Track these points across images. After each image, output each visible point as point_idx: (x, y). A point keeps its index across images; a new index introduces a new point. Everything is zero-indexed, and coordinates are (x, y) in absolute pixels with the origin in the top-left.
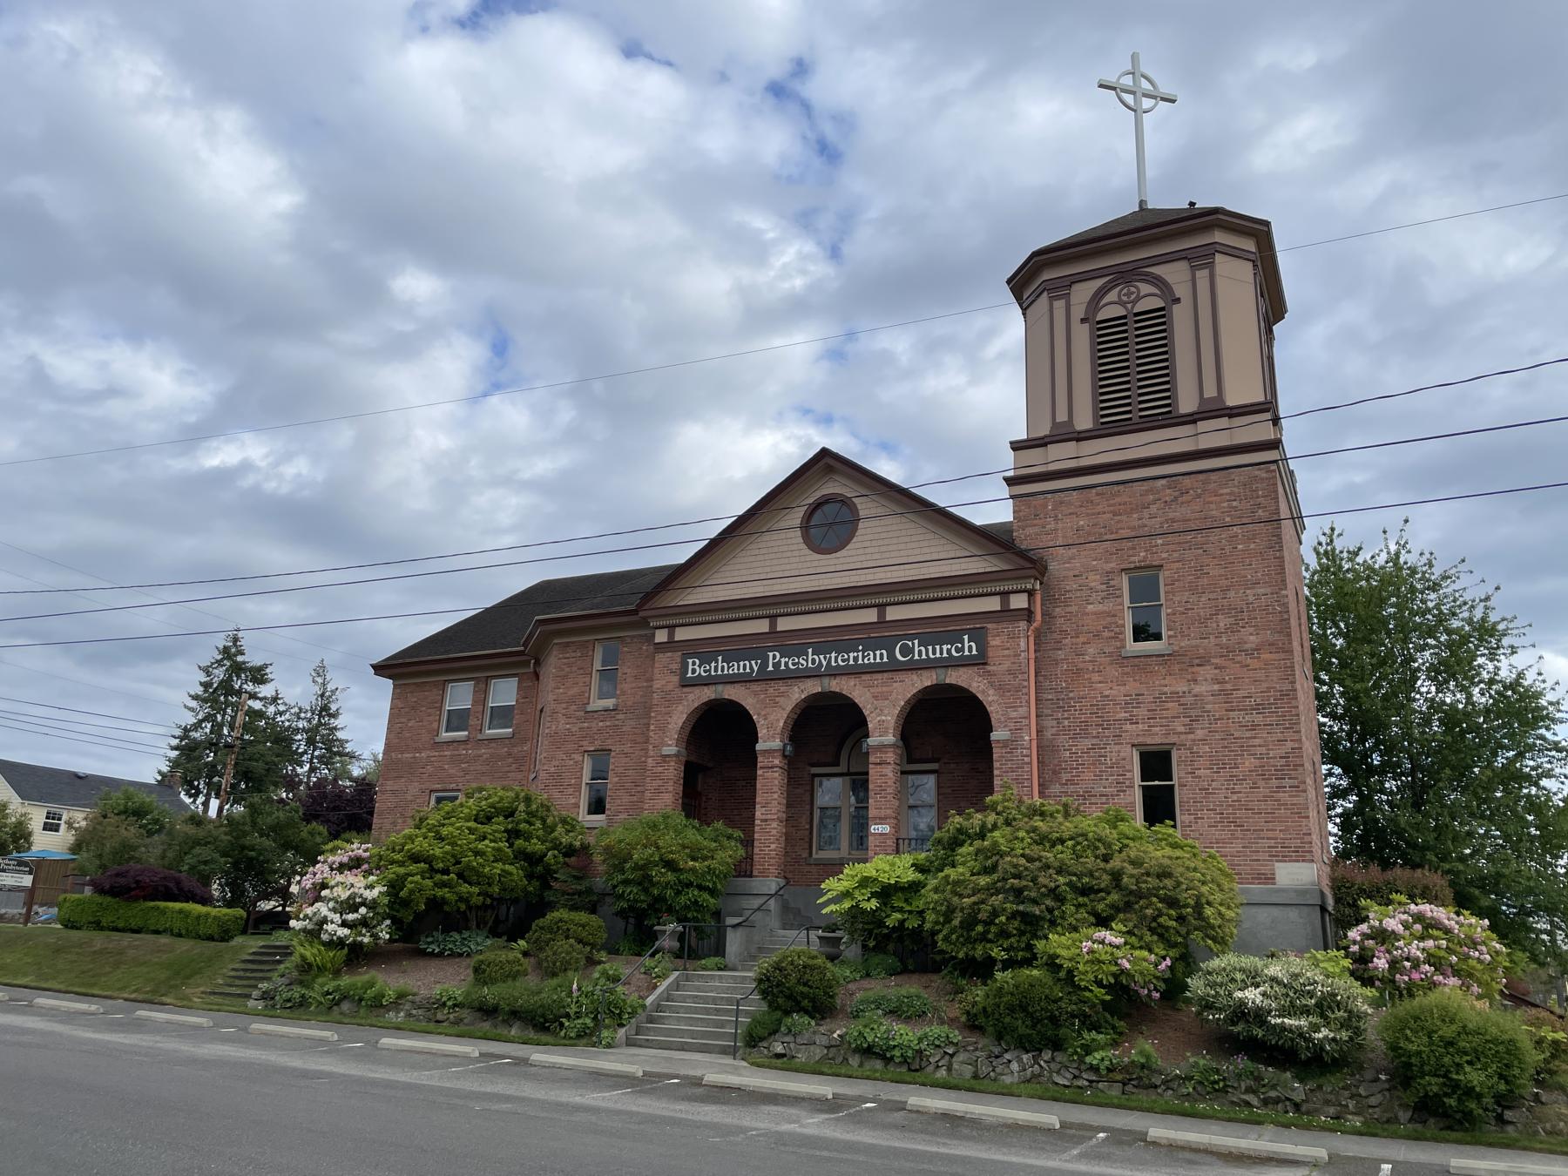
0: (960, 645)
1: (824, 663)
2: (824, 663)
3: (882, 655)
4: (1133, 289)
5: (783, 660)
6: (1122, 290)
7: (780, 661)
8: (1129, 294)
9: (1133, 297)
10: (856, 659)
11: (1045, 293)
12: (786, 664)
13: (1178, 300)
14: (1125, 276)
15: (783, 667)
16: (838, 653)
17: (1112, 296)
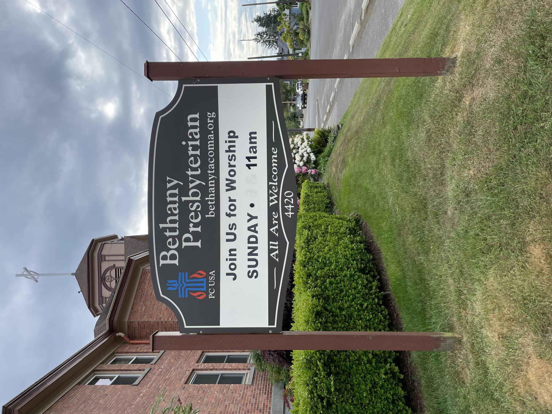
0: (209, 159)
1: (198, 182)
2: (198, 182)
3: (193, 120)
4: (107, 278)
5: (192, 229)
6: (107, 281)
7: (193, 233)
8: (109, 279)
9: (110, 278)
10: (195, 148)
11: (103, 305)
12: (196, 225)
13: (114, 265)
14: (102, 279)
15: (199, 229)
16: (188, 167)
17: (108, 284)
